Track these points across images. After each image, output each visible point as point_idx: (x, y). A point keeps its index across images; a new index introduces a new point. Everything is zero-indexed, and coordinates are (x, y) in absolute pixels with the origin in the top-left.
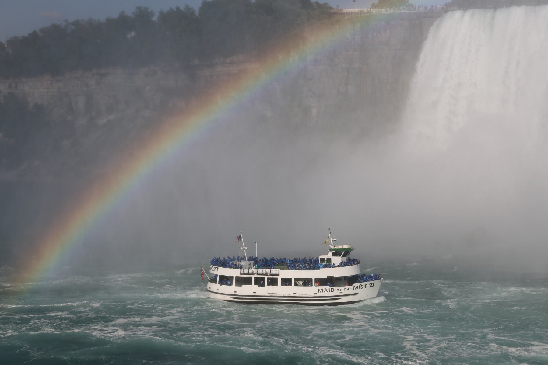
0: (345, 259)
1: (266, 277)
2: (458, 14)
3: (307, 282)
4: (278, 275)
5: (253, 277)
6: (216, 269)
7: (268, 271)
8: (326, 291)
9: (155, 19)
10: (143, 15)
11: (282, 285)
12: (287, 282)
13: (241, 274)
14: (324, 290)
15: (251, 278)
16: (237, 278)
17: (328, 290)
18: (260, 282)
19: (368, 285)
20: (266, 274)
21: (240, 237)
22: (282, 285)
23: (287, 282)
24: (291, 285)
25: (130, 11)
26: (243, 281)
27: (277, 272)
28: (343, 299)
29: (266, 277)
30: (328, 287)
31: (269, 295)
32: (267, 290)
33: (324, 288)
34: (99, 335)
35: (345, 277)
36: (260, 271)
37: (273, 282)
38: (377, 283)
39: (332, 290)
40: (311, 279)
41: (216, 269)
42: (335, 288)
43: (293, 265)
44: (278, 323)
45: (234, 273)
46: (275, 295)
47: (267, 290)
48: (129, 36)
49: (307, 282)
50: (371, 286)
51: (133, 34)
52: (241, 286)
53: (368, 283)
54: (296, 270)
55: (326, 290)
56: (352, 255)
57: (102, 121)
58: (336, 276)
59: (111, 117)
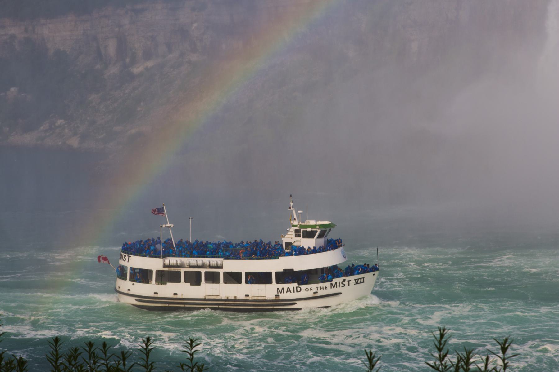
0: (322, 241)
1: (203, 271)
3: (263, 278)
4: (221, 267)
6: (127, 258)
8: (290, 291)
12: (233, 278)
13: (165, 266)
14: (285, 290)
16: (158, 272)
17: (292, 289)
18: (194, 279)
19: (353, 282)
20: (203, 266)
23: (233, 278)
26: (165, 277)
27: (220, 263)
29: (203, 271)
31: (207, 297)
32: (206, 290)
33: (286, 286)
34: (173, 346)
35: (322, 269)
36: (193, 261)
37: (213, 278)
38: (369, 277)
41: (127, 258)
42: (303, 287)
43: (201, 249)
45: (153, 264)
46: (218, 298)
47: (206, 290)
49: (263, 278)
50: (357, 283)
52: (166, 284)
53: (352, 278)
54: (240, 259)
55: (289, 290)
56: (332, 236)
57: (136, 70)
58: (296, 268)
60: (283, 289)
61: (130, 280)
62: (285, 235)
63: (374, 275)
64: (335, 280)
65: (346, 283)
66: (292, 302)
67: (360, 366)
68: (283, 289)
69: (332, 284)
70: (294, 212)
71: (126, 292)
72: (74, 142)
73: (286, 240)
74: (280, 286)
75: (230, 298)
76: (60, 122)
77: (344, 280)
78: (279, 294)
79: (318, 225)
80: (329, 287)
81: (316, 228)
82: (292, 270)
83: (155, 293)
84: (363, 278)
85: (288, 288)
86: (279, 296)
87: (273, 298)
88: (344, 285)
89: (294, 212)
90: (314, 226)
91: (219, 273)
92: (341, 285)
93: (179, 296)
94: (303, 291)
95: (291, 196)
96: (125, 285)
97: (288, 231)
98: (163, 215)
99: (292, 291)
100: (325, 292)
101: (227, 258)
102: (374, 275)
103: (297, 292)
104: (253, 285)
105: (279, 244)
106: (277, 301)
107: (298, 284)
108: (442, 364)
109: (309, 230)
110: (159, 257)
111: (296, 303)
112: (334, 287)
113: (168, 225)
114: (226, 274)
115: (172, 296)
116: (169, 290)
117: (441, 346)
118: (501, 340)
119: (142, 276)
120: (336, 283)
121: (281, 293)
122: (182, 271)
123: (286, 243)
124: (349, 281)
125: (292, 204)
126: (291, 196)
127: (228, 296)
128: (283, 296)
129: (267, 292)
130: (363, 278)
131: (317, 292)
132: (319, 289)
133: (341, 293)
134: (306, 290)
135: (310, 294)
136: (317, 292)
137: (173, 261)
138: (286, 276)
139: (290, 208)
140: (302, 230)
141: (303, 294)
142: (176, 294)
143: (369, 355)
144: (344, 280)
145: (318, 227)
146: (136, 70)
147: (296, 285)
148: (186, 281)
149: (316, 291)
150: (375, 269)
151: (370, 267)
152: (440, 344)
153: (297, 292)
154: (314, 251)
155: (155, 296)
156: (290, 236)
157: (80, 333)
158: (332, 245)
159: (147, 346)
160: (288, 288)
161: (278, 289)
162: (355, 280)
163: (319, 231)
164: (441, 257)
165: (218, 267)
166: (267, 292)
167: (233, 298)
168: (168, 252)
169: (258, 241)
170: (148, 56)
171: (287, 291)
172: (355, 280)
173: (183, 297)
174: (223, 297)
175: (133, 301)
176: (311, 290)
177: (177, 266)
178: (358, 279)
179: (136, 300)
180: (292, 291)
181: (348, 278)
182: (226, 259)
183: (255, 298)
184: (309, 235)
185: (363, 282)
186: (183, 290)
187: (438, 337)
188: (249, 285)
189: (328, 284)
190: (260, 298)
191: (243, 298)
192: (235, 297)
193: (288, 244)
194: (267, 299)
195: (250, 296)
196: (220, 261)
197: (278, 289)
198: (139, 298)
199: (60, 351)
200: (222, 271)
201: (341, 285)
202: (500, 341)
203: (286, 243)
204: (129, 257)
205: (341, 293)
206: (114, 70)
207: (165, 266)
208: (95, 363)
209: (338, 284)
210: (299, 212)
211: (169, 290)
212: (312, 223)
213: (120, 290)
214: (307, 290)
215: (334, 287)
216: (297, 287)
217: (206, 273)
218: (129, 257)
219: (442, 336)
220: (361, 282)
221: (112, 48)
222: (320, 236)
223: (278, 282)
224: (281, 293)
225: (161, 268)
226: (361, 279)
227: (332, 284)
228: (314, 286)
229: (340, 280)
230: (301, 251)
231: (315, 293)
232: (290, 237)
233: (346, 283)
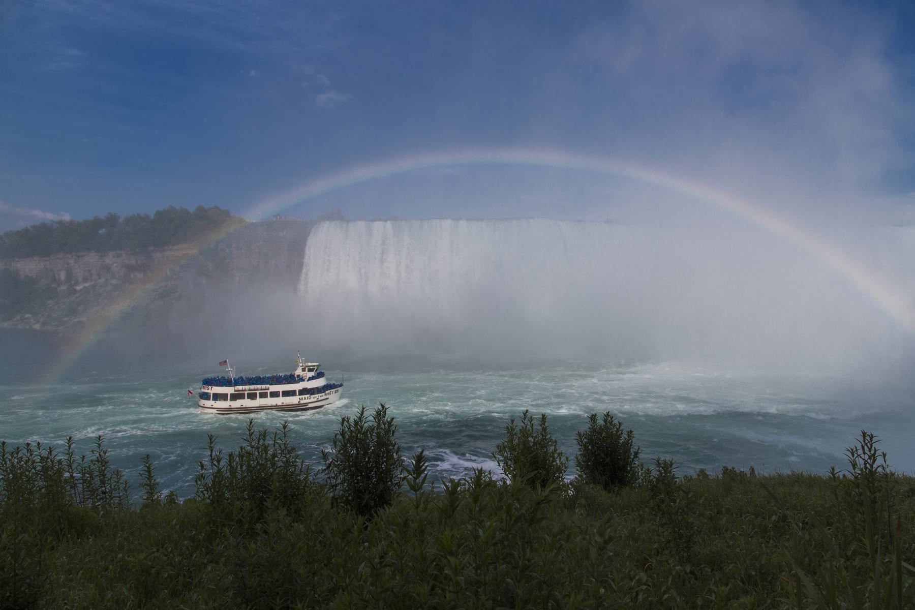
1: (258, 392)
2: (327, 223)
5: (258, 392)
7: (259, 387)
8: (306, 399)
9: (121, 220)
10: (112, 220)
12: (275, 394)
18: (252, 396)
21: (225, 362)
25: (102, 215)
26: (235, 397)
28: (310, 405)
30: (306, 396)
32: (259, 402)
36: (252, 387)
37: (264, 395)
43: (278, 380)
45: (229, 390)
47: (259, 402)
48: (100, 232)
51: (104, 230)
57: (78, 288)
59: (87, 285)
66: (307, 404)
72: (37, 327)
76: (27, 316)
106: (299, 404)
116: (237, 404)
119: (217, 397)
128: (302, 402)
129: (294, 400)
134: (314, 398)
137: (240, 388)
138: (303, 392)
141: (312, 400)
146: (78, 288)
150: (341, 385)
157: (627, 407)
158: (320, 375)
164: (49, 386)
166: (294, 400)
168: (238, 382)
170: (85, 280)
175: (215, 411)
184: (310, 370)
186: (247, 403)
193: (298, 376)
196: (267, 386)
199: (6, 450)
206: (64, 287)
208: (31, 455)
211: (237, 404)
221: (63, 276)
232: (299, 372)
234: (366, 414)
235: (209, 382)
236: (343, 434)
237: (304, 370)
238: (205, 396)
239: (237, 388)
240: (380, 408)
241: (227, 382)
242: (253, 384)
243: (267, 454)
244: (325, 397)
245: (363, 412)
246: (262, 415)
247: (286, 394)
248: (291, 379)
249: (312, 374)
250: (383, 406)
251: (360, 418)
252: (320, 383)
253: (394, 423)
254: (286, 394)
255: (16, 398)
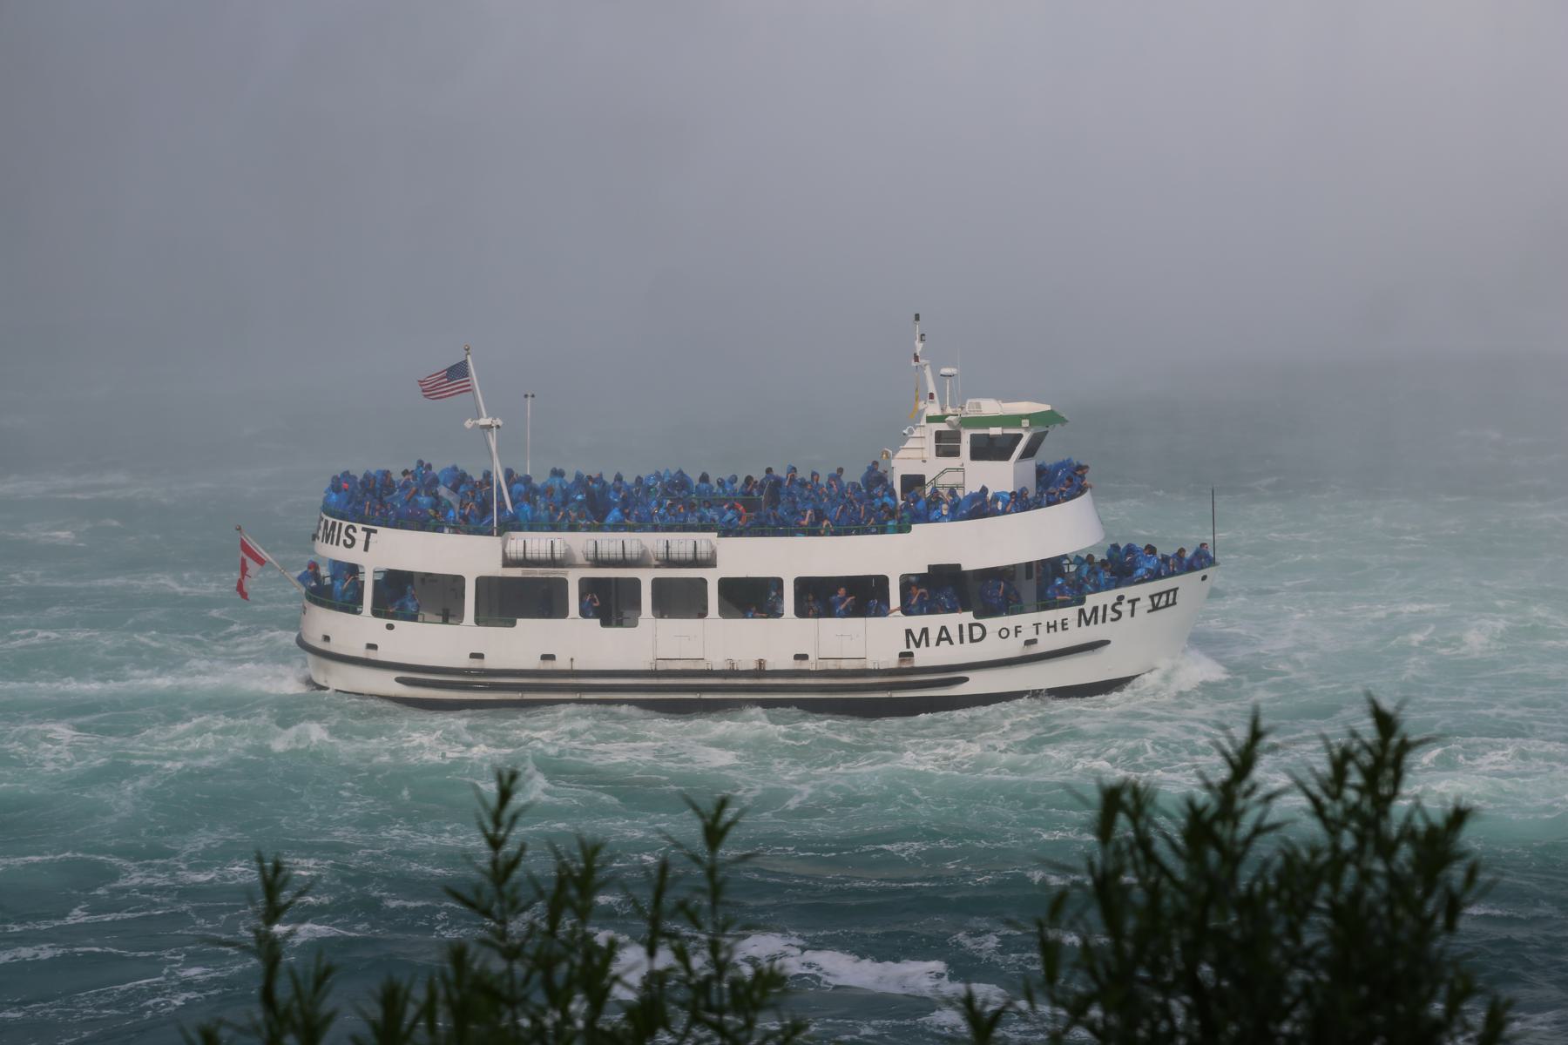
1: (646, 577)
3: (862, 596)
4: (710, 563)
5: (646, 577)
6: (360, 536)
8: (949, 638)
11: (478, 622)
12: (749, 597)
13: (508, 562)
15: (636, 583)
16: (482, 583)
18: (610, 602)
19: (1145, 603)
21: (458, 372)
22: (478, 622)
23: (749, 597)
24: (702, 614)
26: (513, 599)
27: (704, 549)
28: (977, 684)
31: (662, 666)
32: (652, 641)
33: (934, 622)
34: (909, 756)
36: (610, 542)
37: (680, 599)
39: (977, 632)
40: (778, 583)
41: (360, 536)
42: (993, 624)
43: (771, 507)
44: (291, 934)
45: (469, 556)
46: (702, 666)
47: (652, 641)
49: (862, 596)
50: (1155, 608)
53: (1143, 591)
55: (944, 636)
56: (1049, 454)
60: (925, 631)
61: (376, 613)
62: (896, 451)
63: (1204, 578)
64: (1092, 600)
65: (1125, 607)
66: (954, 673)
67: (83, 920)
68: (925, 631)
69: (1082, 612)
70: (928, 372)
71: (360, 652)
73: (903, 464)
74: (917, 623)
75: (742, 667)
77: (1121, 598)
78: (913, 648)
79: (1027, 416)
80: (1073, 624)
81: (1019, 425)
82: (959, 566)
83: (473, 656)
84: (1175, 590)
85: (944, 628)
86: (911, 654)
87: (892, 662)
88: (1120, 614)
89: (928, 372)
90: (1015, 420)
91: (703, 582)
92: (1110, 614)
93: (561, 664)
94: (992, 636)
95: (917, 317)
96: (355, 630)
97: (905, 438)
98: (468, 389)
99: (956, 639)
100: (1047, 642)
101: (727, 531)
102: (1204, 578)
103: (972, 640)
104: (869, 620)
105: (876, 478)
106: (905, 672)
107: (976, 616)
108: (501, 895)
109: (995, 431)
110: (491, 534)
111: (966, 679)
112: (1088, 623)
113: (484, 421)
114: (726, 585)
115: (534, 663)
116: (521, 644)
117: (501, 833)
118: (708, 806)
119: (402, 595)
120: (1095, 609)
121: (918, 645)
122: (573, 577)
123: (904, 478)
124: (1133, 602)
125: (919, 346)
126: (917, 317)
127: (735, 659)
128: (925, 656)
129: (872, 642)
130: (1175, 590)
131: (1034, 641)
132: (1043, 629)
133: (1108, 642)
134: (1003, 634)
135: (1014, 648)
136: (1034, 641)
137: (538, 543)
138: (941, 588)
139: (916, 359)
140: (966, 436)
141: (992, 648)
142: (551, 657)
143: (269, 874)
144: (1121, 598)
145: (1025, 423)
147: (967, 617)
148: (584, 613)
149: (1032, 636)
151: (1188, 554)
152: (497, 822)
153: (972, 640)
154: (1020, 502)
155: (476, 664)
156: (917, 454)
158: (1056, 484)
159: (495, 843)
160: (944, 628)
161: (909, 632)
162: (1152, 597)
163: (1026, 437)
165: (695, 563)
166: (872, 642)
167: (753, 666)
169: (781, 472)
171: (940, 639)
172: (1152, 597)
173: (577, 667)
174: (718, 664)
176: (1017, 632)
177: (552, 562)
178: (1160, 595)
179: (398, 680)
180: (956, 639)
181: (1129, 592)
182: (725, 533)
183: (831, 665)
184: (988, 449)
185: (1174, 603)
186: (578, 641)
187: (493, 801)
188: (810, 622)
189: (1071, 613)
190: (845, 665)
191: (789, 664)
192: (761, 662)
193: (913, 483)
194: (870, 666)
195: (812, 658)
196: (706, 541)
197: (909, 632)
198: (410, 672)
200: (712, 577)
201: (1110, 614)
202: (703, 810)
203: (904, 478)
204: (369, 532)
205: (1108, 642)
207: (508, 562)
209: (1100, 613)
210: (945, 371)
211: (521, 644)
212: (990, 407)
213: (333, 647)
214: (1003, 634)
215: (1088, 623)
216: (971, 626)
217: (657, 584)
218: (369, 532)
219: (505, 795)
220: (1167, 605)
222: (1029, 453)
223: (907, 610)
224: (918, 645)
225: (495, 569)
226: (1168, 592)
227: (1082, 612)
228: (1026, 620)
229: (1106, 598)
230: (980, 507)
231: (1028, 643)
232: (915, 457)
233: (1125, 607)
234: (1268, 774)
235: (372, 500)
236: (1106, 889)
237: (946, 445)
238: (337, 589)
239: (518, 542)
240: (1368, 729)
241: (473, 509)
242: (645, 524)
243: (598, 998)
244: (1078, 635)
245: (1243, 764)
246: (550, 733)
247: (819, 596)
248: (879, 505)
249: (1000, 476)
250: (1385, 723)
251: (1227, 793)
252: (1063, 531)
253: (1470, 838)
254: (819, 596)
255: (115, 523)
